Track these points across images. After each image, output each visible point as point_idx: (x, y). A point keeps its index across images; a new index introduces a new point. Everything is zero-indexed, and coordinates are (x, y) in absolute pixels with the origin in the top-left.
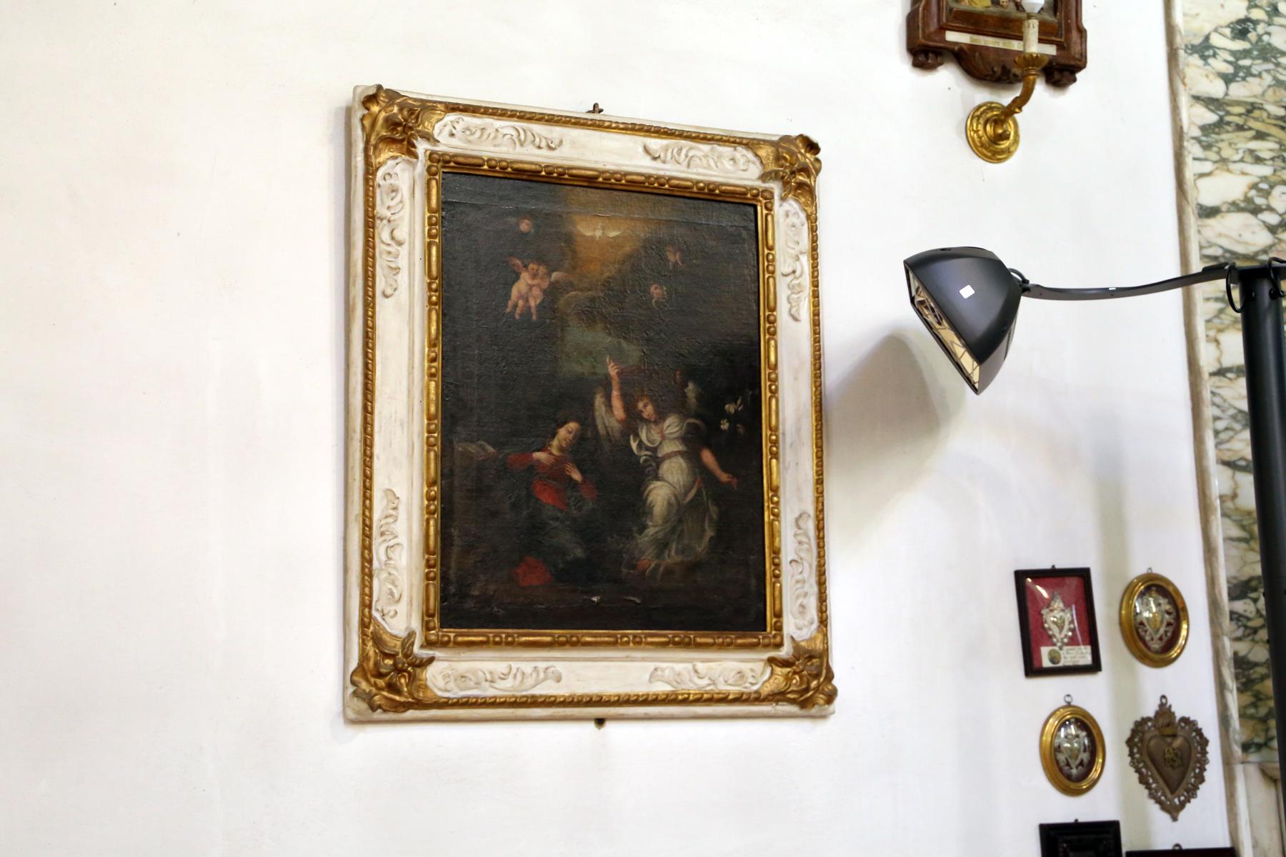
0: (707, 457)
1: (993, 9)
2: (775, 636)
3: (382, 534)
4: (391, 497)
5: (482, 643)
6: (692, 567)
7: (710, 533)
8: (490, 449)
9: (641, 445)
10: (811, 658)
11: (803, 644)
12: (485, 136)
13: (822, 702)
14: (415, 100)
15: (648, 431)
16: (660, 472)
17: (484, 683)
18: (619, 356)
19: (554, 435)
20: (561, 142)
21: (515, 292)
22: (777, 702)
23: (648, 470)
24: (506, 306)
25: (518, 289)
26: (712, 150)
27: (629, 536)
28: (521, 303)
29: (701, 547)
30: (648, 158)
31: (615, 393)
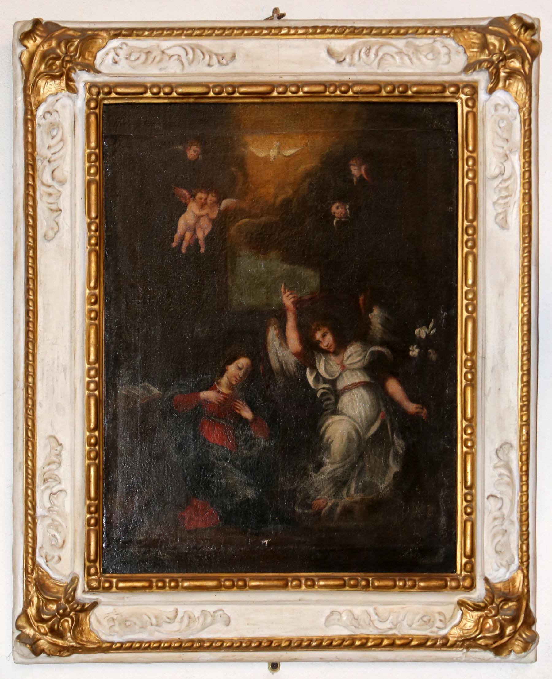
0: (394, 387)
1: (243, 371)
2: (465, 578)
3: (45, 481)
4: (54, 444)
5: (144, 588)
6: (374, 506)
7: (394, 468)
8: (156, 391)
9: (318, 377)
10: (507, 600)
11: (499, 586)
12: (150, 60)
13: (517, 649)
14: (75, 30)
15: (327, 363)
16: (340, 406)
17: (149, 627)
18: (292, 283)
19: (223, 371)
20: (234, 57)
21: (182, 224)
22: (468, 648)
23: (327, 402)
24: (172, 240)
25: (184, 222)
26: (407, 45)
27: (304, 474)
28: (188, 235)
29: (384, 485)
30: (333, 62)
31: (291, 324)
